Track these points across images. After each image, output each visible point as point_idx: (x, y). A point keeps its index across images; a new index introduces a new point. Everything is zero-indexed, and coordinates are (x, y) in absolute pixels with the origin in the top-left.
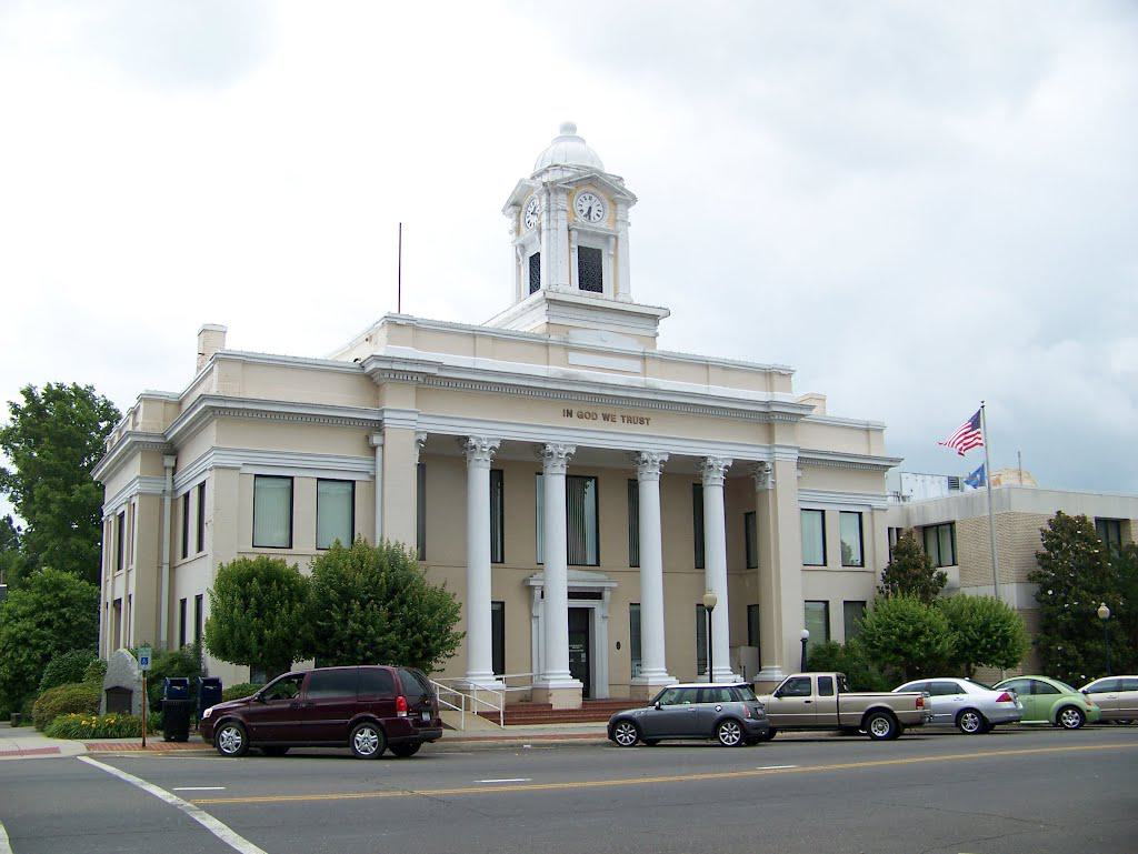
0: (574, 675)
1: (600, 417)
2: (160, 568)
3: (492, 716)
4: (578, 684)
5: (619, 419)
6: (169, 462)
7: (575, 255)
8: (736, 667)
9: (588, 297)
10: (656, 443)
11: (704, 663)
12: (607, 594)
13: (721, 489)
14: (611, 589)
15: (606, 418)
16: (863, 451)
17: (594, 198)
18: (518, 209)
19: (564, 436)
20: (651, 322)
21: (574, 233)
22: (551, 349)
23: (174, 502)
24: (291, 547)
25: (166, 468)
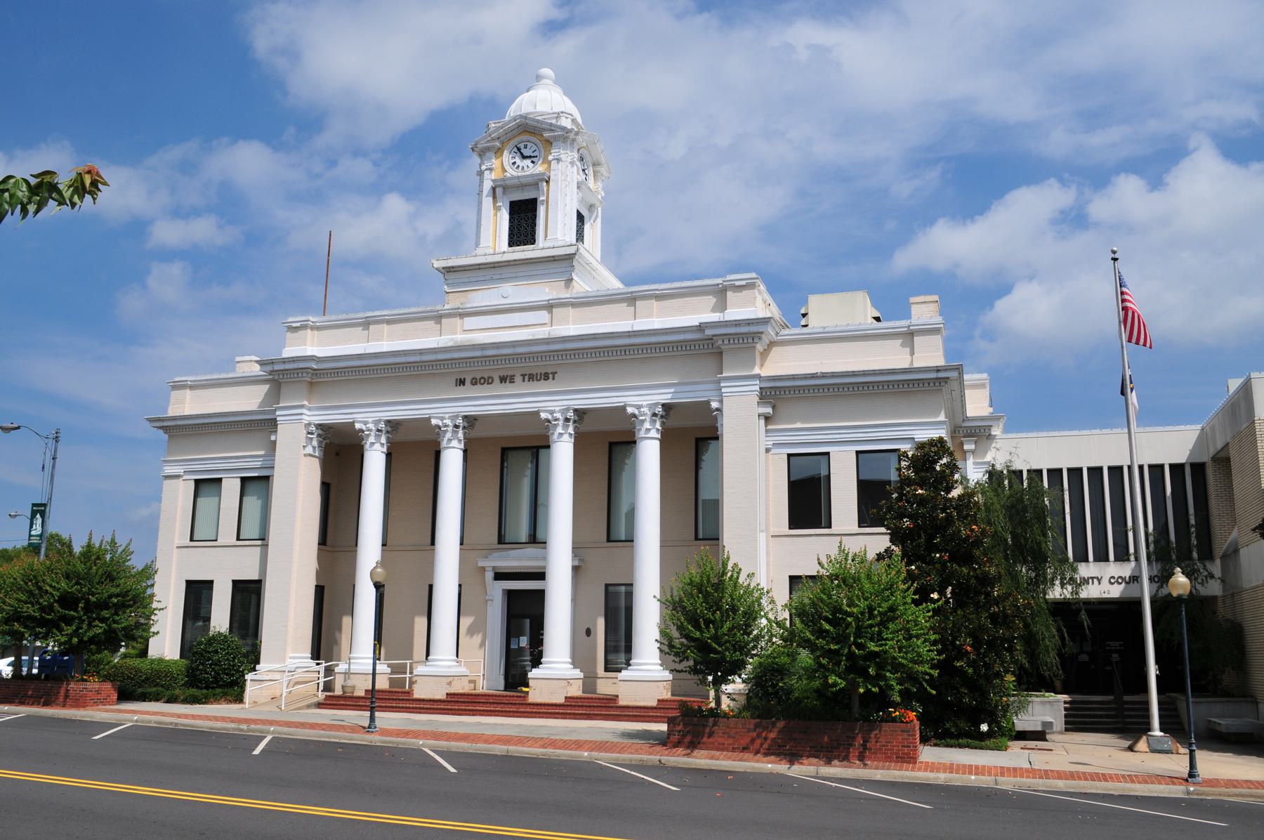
0: (575, 664)
1: (497, 380)
4: (578, 673)
5: (518, 379)
7: (505, 216)
8: (579, 657)
11: (620, 645)
13: (658, 442)
15: (503, 379)
16: (904, 364)
17: (529, 145)
20: (565, 264)
21: (499, 191)
22: (918, 340)
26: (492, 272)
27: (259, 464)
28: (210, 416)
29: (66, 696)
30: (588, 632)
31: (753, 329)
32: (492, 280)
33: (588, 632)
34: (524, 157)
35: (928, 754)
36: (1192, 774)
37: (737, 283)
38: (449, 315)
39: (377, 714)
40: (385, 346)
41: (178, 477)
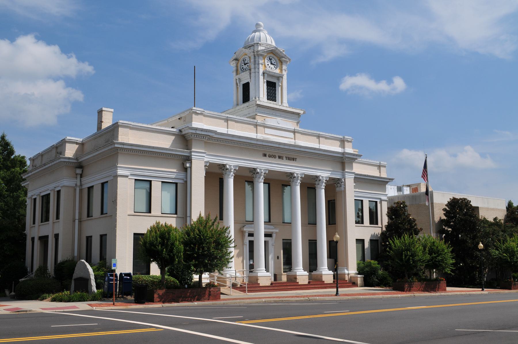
1: (277, 157)
2: (74, 221)
3: (242, 289)
4: (331, 272)
5: (284, 158)
6: (79, 171)
9: (271, 104)
10: (299, 170)
11: (243, 269)
12: (274, 235)
14: (276, 233)
15: (280, 157)
16: (378, 176)
18: (237, 62)
19: (263, 166)
20: (297, 116)
21: (266, 75)
23: (81, 190)
24: (150, 212)
25: (77, 174)
26: (273, 111)
27: (174, 176)
28: (153, 148)
29: (210, 295)
30: (278, 258)
31: (355, 157)
32: (272, 115)
33: (278, 258)
34: (272, 64)
35: (448, 289)
36: (337, 294)
37: (198, 112)
38: (260, 126)
39: (339, 289)
40: (324, 147)
41: (127, 176)
